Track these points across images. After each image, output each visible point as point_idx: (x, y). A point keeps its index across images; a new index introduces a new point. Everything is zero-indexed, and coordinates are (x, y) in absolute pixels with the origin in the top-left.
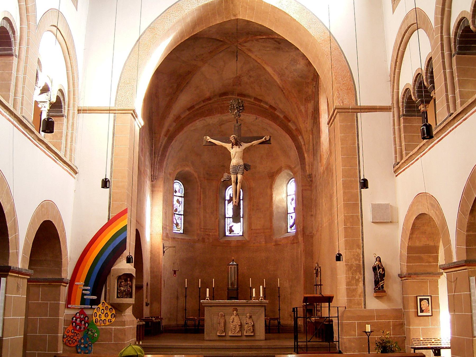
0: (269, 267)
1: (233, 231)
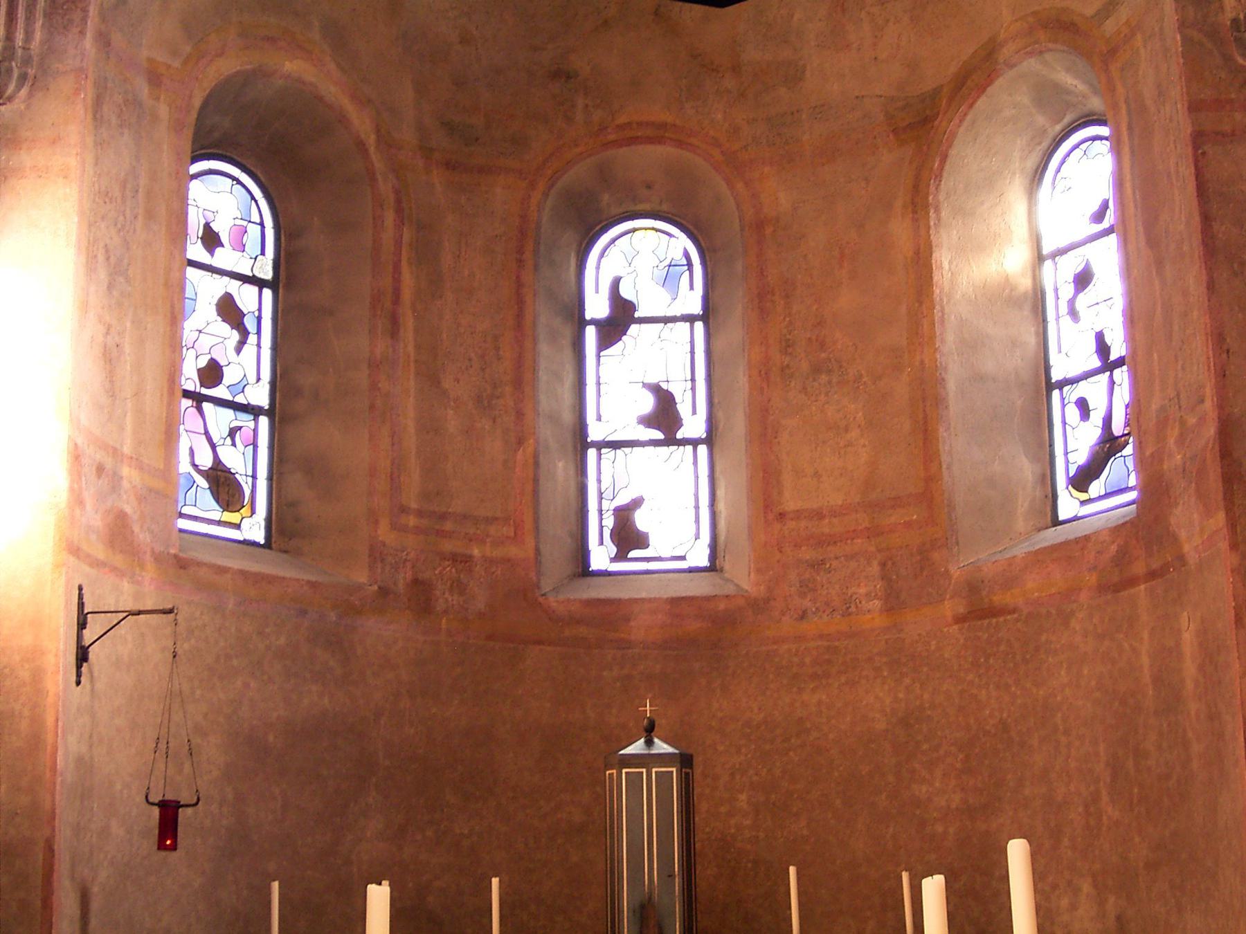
0: (922, 790)
1: (640, 541)
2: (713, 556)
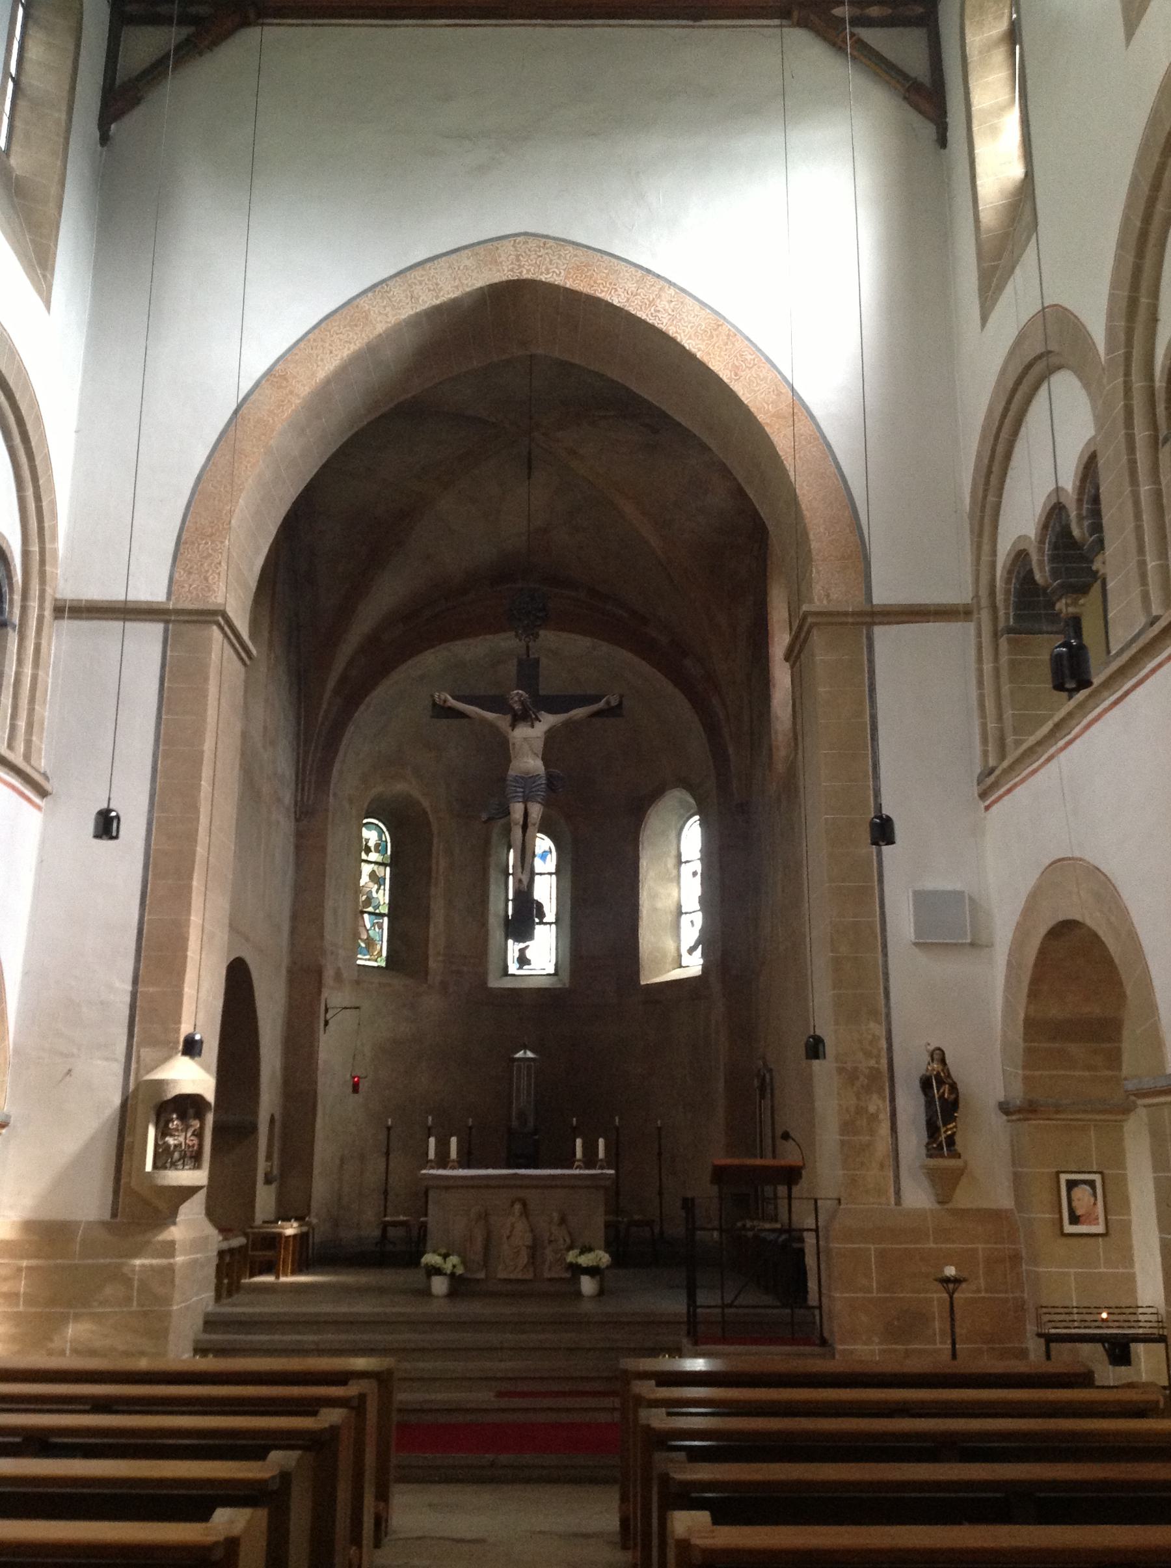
1: (528, 962)
2: (556, 969)
